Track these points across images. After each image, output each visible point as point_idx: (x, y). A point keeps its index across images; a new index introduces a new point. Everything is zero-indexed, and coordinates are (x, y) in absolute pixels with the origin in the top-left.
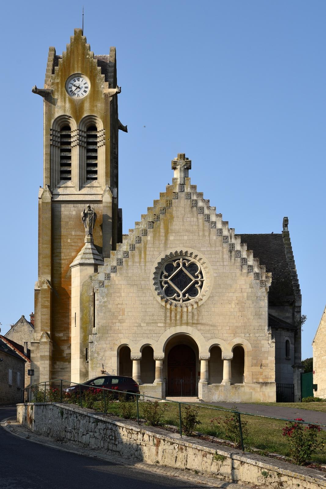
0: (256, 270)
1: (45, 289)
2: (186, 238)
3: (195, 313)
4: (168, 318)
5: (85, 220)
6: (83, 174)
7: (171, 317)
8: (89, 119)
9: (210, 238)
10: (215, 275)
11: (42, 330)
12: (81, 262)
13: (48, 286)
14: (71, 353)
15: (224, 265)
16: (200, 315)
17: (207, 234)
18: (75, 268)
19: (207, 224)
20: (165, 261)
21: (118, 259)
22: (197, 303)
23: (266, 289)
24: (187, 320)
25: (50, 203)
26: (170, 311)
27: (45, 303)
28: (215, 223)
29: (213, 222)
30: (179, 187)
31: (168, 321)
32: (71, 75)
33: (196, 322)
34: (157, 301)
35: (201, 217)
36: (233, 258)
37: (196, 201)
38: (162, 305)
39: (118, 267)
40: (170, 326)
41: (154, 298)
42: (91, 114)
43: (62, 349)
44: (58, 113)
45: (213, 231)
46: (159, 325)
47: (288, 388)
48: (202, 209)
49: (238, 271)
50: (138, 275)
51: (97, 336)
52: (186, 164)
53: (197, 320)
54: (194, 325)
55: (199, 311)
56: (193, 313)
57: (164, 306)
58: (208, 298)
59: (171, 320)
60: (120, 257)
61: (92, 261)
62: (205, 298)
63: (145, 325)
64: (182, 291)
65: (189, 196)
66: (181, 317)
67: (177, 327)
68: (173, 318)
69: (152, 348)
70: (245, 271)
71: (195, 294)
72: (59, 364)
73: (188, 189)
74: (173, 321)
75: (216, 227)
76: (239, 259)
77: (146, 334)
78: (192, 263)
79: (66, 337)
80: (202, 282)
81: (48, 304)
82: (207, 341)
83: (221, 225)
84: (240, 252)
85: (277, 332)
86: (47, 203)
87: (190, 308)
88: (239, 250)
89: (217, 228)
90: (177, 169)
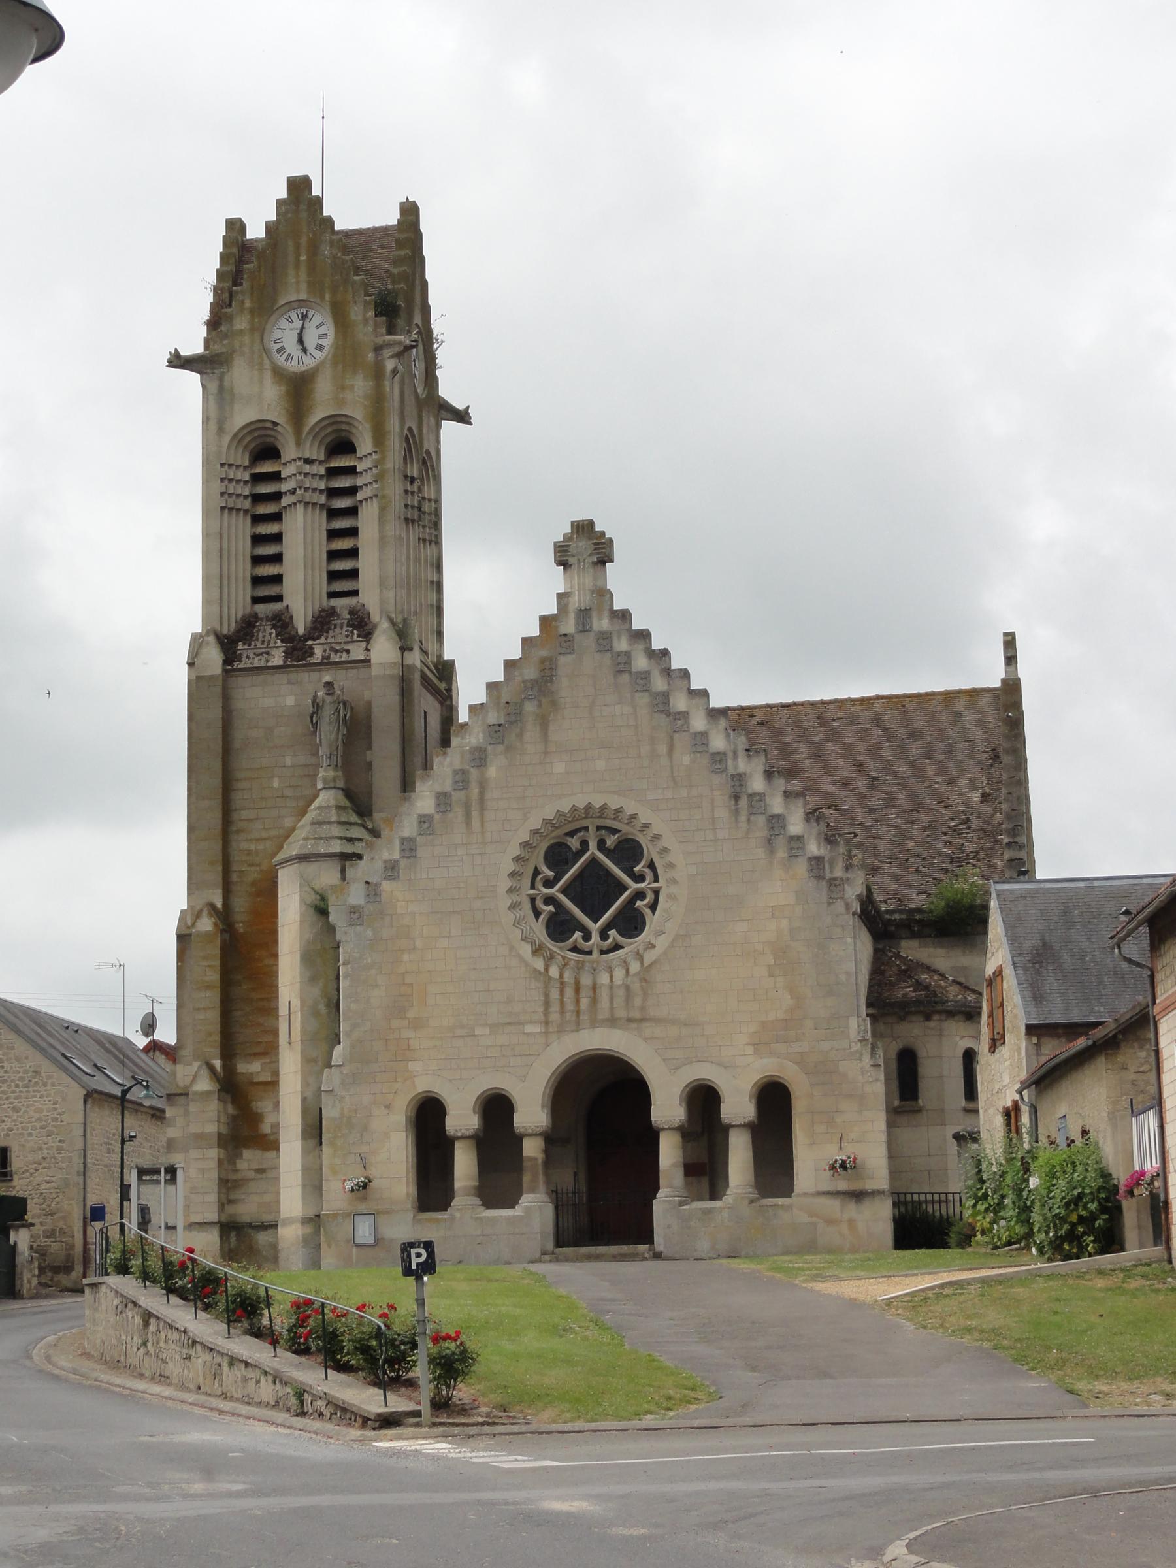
0: (814, 848)
1: (207, 934)
2: (600, 765)
3: (636, 987)
4: (555, 1008)
5: (316, 722)
6: (317, 581)
7: (562, 1003)
8: (332, 424)
9: (671, 762)
10: (693, 870)
11: (196, 1057)
12: (309, 848)
13: (215, 924)
14: (279, 1124)
15: (716, 840)
16: (650, 992)
17: (663, 749)
18: (286, 868)
19: (663, 720)
20: (542, 838)
21: (403, 840)
22: (639, 957)
23: (848, 906)
24: (612, 1008)
25: (221, 678)
26: (558, 985)
27: (206, 975)
28: (684, 716)
29: (679, 713)
30: (577, 618)
31: (555, 1016)
32: (280, 305)
33: (637, 1014)
34: (519, 956)
35: (643, 700)
36: (743, 818)
37: (628, 654)
38: (535, 970)
39: (403, 864)
40: (561, 1030)
41: (512, 948)
42: (341, 413)
43: (259, 1111)
44: (242, 416)
45: (682, 741)
46: (529, 1029)
47: (940, 1202)
48: (646, 676)
49: (760, 853)
50: (462, 885)
51: (345, 1070)
52: (595, 549)
53: (643, 1008)
54: (634, 1025)
55: (646, 981)
56: (627, 988)
57: (540, 973)
58: (673, 941)
59: (562, 1011)
60: (407, 832)
61: (337, 847)
62: (662, 943)
63: (487, 1031)
64: (596, 922)
65: (605, 639)
66: (594, 1001)
67: (583, 1031)
68: (570, 1007)
69: (444, 1107)
70: (781, 854)
71: (636, 928)
72: (249, 1158)
73: (602, 623)
74: (568, 1016)
75: (688, 727)
76: (761, 820)
77: (489, 1059)
78: (623, 838)
79: (269, 1074)
80: (656, 893)
81: (214, 977)
82: (672, 1071)
83: (705, 722)
84: (761, 797)
85: (932, 1024)
86: (211, 677)
87: (619, 974)
88: (757, 791)
89: (691, 731)
90: (571, 565)
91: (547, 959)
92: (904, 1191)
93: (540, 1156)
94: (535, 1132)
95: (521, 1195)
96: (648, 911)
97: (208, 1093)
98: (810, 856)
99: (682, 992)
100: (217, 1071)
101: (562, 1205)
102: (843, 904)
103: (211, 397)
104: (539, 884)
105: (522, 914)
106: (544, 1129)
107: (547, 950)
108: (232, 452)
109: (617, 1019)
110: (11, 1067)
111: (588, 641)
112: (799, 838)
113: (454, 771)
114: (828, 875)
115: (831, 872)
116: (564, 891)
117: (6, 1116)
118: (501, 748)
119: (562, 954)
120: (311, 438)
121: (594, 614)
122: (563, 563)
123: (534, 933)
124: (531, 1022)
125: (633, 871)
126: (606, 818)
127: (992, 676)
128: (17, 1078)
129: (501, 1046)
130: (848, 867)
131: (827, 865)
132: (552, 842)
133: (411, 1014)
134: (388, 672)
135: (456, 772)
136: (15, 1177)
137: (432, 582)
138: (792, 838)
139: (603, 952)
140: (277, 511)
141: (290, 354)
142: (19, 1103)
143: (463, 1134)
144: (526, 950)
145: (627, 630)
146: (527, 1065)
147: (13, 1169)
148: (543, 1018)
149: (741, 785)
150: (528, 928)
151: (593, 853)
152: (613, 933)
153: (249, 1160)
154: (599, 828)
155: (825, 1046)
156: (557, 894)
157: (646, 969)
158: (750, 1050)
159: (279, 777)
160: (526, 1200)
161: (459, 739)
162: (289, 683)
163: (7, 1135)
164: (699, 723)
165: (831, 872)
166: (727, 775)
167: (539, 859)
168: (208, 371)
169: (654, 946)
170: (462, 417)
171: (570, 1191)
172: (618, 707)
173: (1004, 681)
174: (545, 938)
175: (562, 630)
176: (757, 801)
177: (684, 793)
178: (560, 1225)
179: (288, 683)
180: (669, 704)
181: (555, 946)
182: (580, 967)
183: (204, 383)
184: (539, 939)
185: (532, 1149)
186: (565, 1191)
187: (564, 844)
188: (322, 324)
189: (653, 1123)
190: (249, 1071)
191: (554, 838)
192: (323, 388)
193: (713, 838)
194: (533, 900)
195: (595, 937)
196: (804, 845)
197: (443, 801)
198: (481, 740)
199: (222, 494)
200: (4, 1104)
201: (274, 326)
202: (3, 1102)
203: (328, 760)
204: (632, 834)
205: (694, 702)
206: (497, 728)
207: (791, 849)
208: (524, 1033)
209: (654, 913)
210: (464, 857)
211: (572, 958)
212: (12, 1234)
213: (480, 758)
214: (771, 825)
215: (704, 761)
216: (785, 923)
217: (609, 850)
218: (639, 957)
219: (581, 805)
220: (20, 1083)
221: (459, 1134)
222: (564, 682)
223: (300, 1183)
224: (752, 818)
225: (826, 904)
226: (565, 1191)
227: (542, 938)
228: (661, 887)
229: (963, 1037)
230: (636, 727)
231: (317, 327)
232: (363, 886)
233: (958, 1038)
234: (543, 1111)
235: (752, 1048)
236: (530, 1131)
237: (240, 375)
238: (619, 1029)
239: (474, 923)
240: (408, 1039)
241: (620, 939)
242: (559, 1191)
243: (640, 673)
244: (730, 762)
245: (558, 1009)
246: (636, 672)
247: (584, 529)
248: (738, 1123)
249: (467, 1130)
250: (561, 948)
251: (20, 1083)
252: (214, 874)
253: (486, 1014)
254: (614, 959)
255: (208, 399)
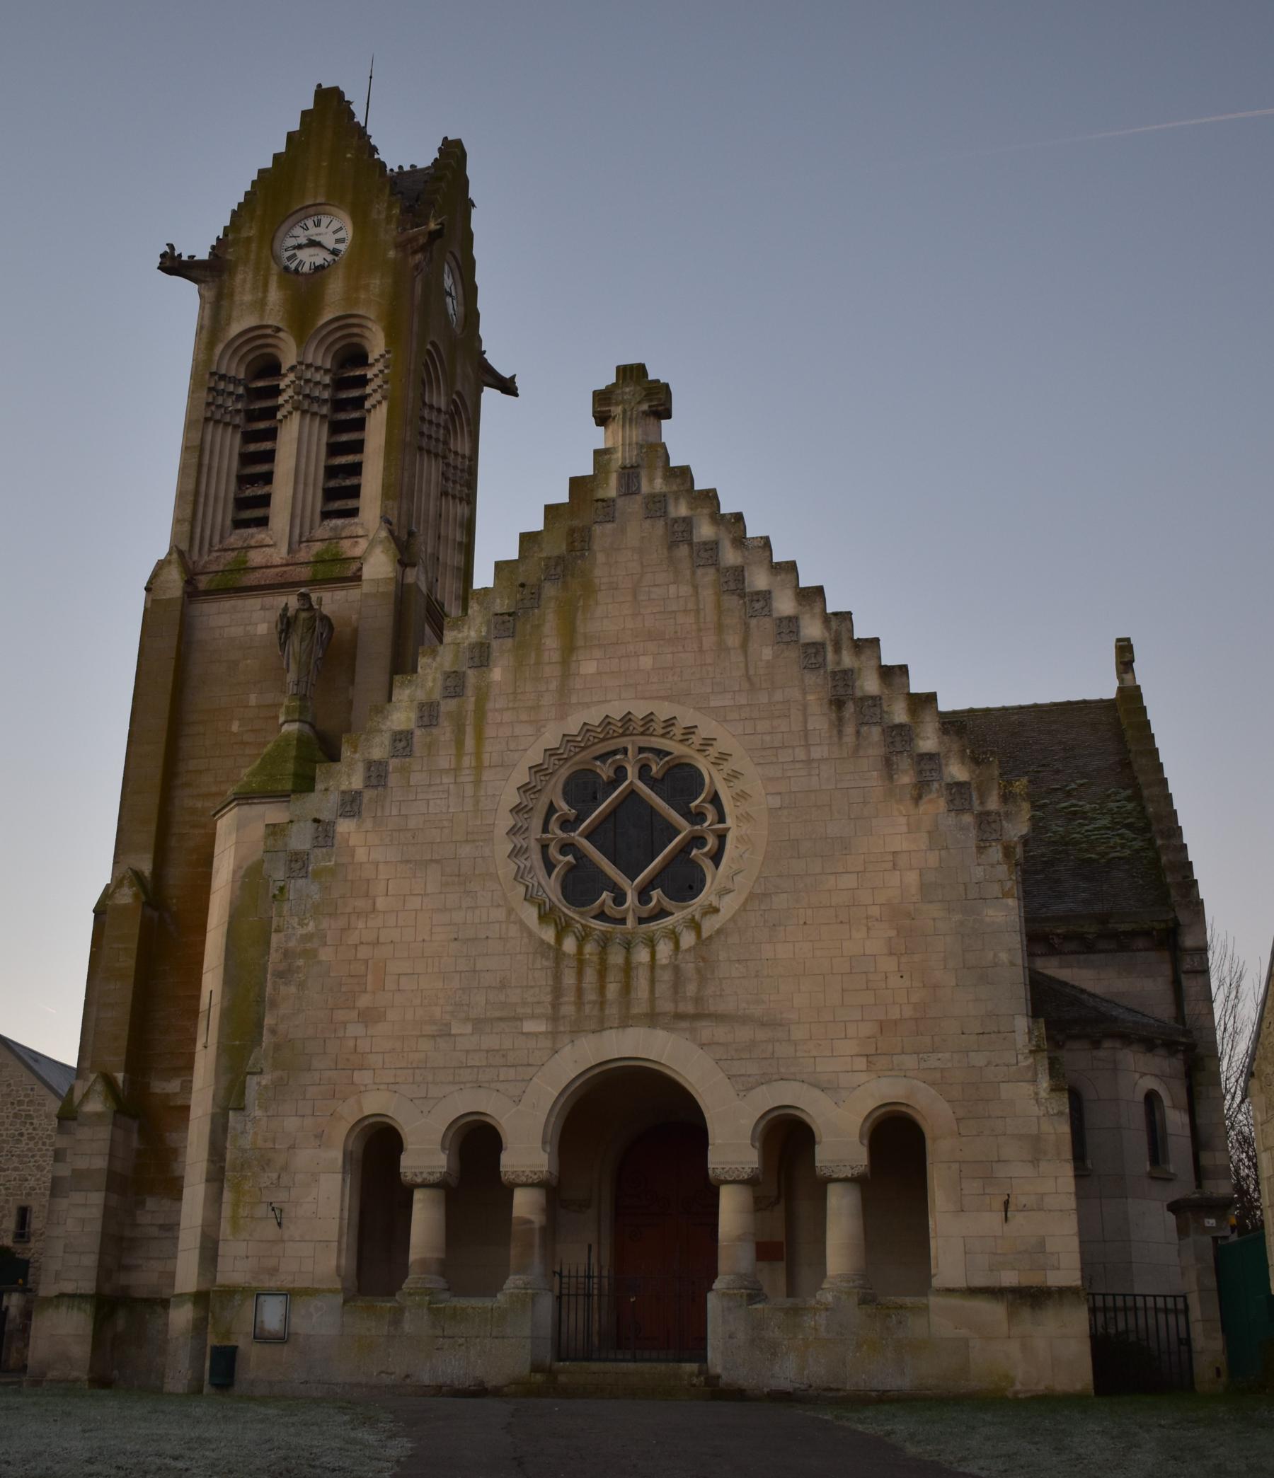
2: (646, 662)
3: (689, 968)
4: (569, 997)
7: (580, 991)
10: (775, 802)
13: (136, 896)
15: (809, 761)
16: (709, 976)
17: (733, 640)
21: (370, 764)
22: (695, 925)
24: (652, 999)
26: (574, 964)
29: (758, 593)
30: (620, 477)
31: (568, 1009)
33: (690, 1008)
34: (522, 924)
35: (707, 577)
36: (850, 730)
38: (542, 942)
39: (368, 795)
40: (577, 1030)
41: (510, 911)
45: (762, 627)
46: (529, 1026)
47: (1125, 1309)
48: (712, 547)
49: (874, 779)
50: (446, 824)
53: (698, 1000)
54: (684, 1024)
55: (704, 959)
56: (676, 969)
57: (549, 945)
60: (377, 754)
62: (729, 906)
65: (656, 506)
66: (627, 988)
68: (591, 996)
70: (906, 779)
74: (587, 1008)
76: (875, 733)
80: (722, 838)
82: (742, 1094)
84: (875, 700)
85: (1101, 1054)
90: (614, 418)
91: (560, 927)
92: (1103, 1291)
93: (538, 1219)
94: (530, 1181)
95: (507, 1278)
96: (707, 865)
97: (98, 1115)
98: (949, 780)
99: (757, 976)
100: (118, 1086)
101: (569, 1295)
102: (999, 847)
103: (207, 306)
104: (554, 826)
105: (528, 865)
106: (544, 1176)
107: (561, 915)
108: (227, 357)
109: (659, 1014)
110: (40, 1124)
111: (634, 506)
112: (931, 757)
113: (445, 673)
114: (977, 807)
115: (982, 803)
116: (589, 836)
117: (30, 1175)
118: (509, 643)
119: (583, 922)
120: (323, 351)
121: (644, 474)
122: (602, 419)
123: (544, 892)
124: (533, 1017)
125: (689, 808)
126: (651, 735)
127: (1105, 687)
128: (44, 1136)
129: (487, 1051)
130: (1006, 798)
131: (975, 795)
132: (574, 769)
133: (364, 1001)
134: (381, 590)
135: (447, 675)
136: (33, 1239)
137: (460, 544)
138: (922, 756)
139: (641, 921)
140: (273, 426)
141: (301, 261)
142: (44, 1161)
143: (425, 1179)
144: (530, 914)
145: (687, 491)
146: (523, 1080)
147: (32, 1230)
148: (550, 1011)
149: (847, 685)
150: (536, 884)
151: (631, 782)
152: (656, 894)
153: (153, 1212)
154: (641, 750)
155: (978, 1059)
156: (577, 838)
157: (703, 942)
158: (861, 1063)
159: (240, 720)
160: (513, 1282)
161: (455, 633)
162: (263, 608)
163: (28, 1194)
164: (785, 605)
165: (982, 803)
166: (825, 672)
167: (554, 792)
168: (208, 279)
169: (716, 910)
170: (508, 387)
171: (581, 1273)
172: (672, 589)
173: (1120, 690)
174: (558, 899)
175: (601, 494)
176: (869, 706)
177: (763, 698)
178: (564, 1329)
179: (261, 609)
180: (743, 583)
181: (575, 912)
182: (605, 943)
183: (202, 292)
184: (550, 900)
185: (525, 1204)
186: (573, 1273)
187: (591, 771)
188: (340, 229)
189: (710, 1172)
190: (166, 1091)
191: (576, 764)
192: (335, 288)
193: (804, 758)
194: (545, 848)
195: (631, 898)
196: (940, 766)
197: (428, 714)
198: (483, 634)
199: (208, 404)
200: (30, 1162)
201: (287, 234)
202: (28, 1160)
203: (295, 687)
204: (691, 757)
205: (779, 578)
206: (506, 617)
207: (921, 772)
208: (523, 1033)
209: (717, 866)
210: (451, 786)
211: (597, 927)
212: (5, 1298)
213: (481, 655)
214: (890, 740)
215: (792, 654)
216: (912, 878)
217: (656, 779)
218: (695, 925)
219: (617, 715)
220: (48, 1141)
221: (419, 1180)
222: (601, 558)
223: (198, 1245)
224: (864, 729)
225: (974, 850)
226: (573, 1273)
227: (554, 899)
228: (728, 829)
229: (1143, 1075)
230: (698, 611)
231: (335, 232)
232: (310, 823)
233: (1137, 1075)
234: (544, 1151)
235: (864, 1059)
236: (524, 1179)
237: (243, 283)
238: (664, 1029)
239: (459, 875)
240: (356, 1038)
241: (668, 904)
242: (565, 1273)
243: (705, 543)
244: (830, 656)
245: (573, 999)
246: (699, 543)
247: (632, 374)
248: (842, 1176)
249: (431, 1173)
250: (582, 914)
251: (48, 1141)
252: (147, 835)
253: (468, 1005)
254: (657, 930)
255: (204, 308)
